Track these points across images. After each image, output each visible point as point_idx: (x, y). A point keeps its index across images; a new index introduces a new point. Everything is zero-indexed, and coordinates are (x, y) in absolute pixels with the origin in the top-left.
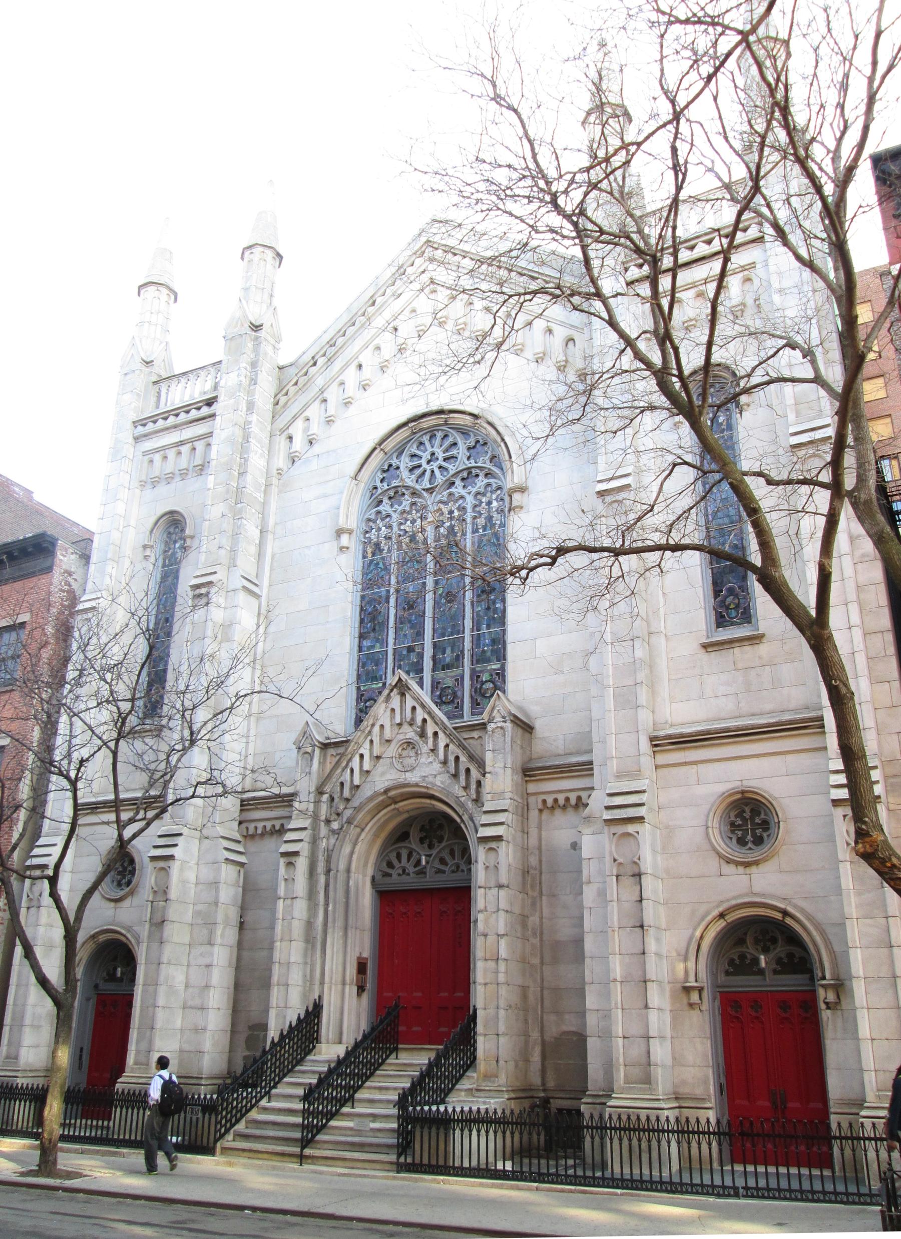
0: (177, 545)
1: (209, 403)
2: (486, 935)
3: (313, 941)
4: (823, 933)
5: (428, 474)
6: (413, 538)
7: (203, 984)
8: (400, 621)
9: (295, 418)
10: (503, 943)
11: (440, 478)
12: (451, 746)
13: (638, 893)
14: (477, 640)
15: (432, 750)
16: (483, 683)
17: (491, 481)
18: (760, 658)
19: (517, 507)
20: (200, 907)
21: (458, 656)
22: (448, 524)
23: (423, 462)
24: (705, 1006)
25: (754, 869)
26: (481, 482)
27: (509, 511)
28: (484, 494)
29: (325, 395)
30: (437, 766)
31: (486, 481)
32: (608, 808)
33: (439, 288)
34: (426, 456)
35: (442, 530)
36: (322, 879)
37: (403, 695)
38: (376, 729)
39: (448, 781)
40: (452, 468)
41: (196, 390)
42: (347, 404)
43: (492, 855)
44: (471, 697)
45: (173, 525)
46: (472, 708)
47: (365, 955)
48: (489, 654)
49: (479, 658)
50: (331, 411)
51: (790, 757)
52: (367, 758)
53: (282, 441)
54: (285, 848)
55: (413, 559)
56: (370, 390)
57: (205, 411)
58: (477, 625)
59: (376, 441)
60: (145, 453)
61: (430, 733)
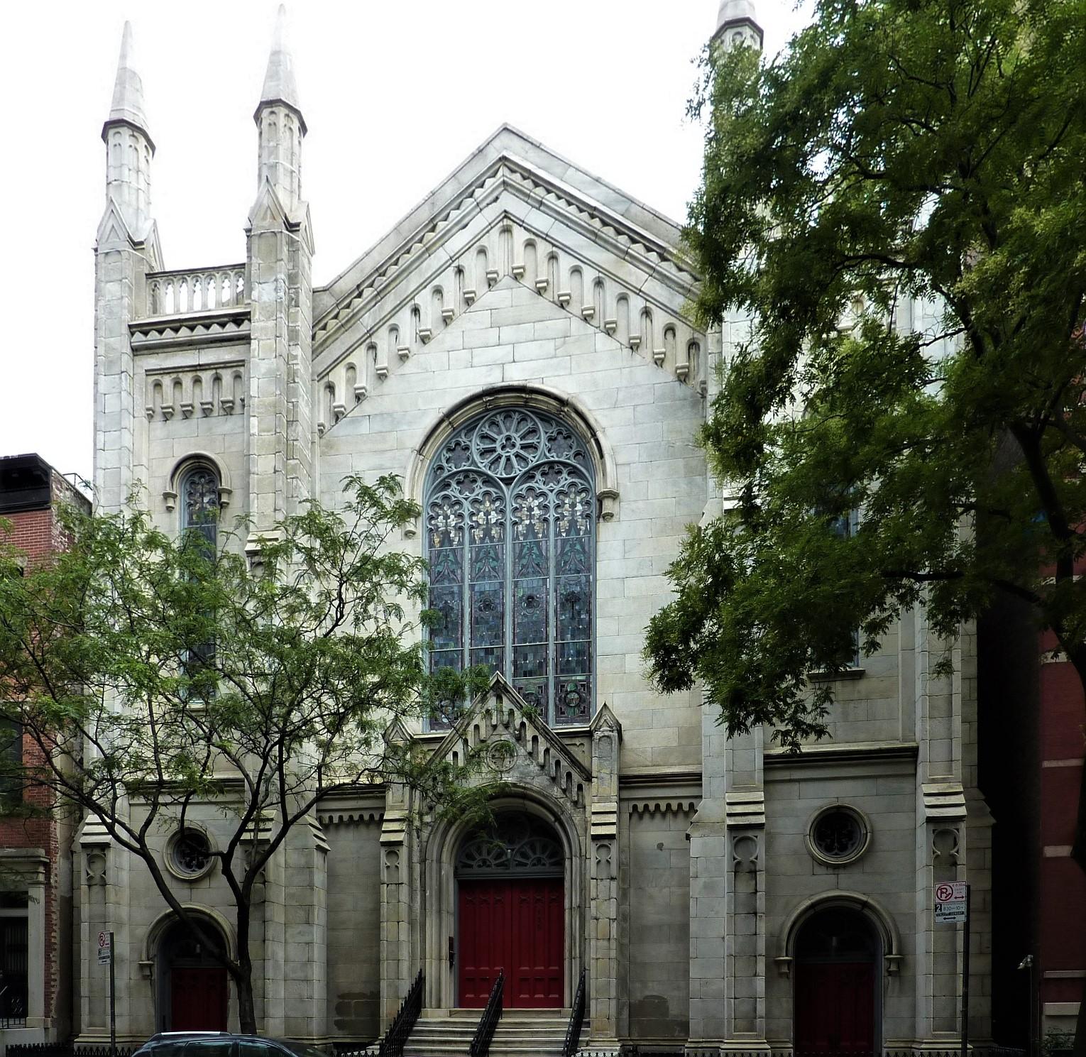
0: (206, 500)
1: (238, 319)
2: (597, 919)
3: (417, 926)
4: (894, 920)
5: (503, 460)
6: (487, 532)
7: (305, 959)
8: (476, 622)
9: (336, 362)
10: (614, 925)
11: (518, 469)
12: (552, 751)
13: (753, 887)
14: (561, 649)
15: (530, 754)
16: (567, 693)
17: (491, 490)
18: (859, 692)
19: (608, 514)
20: (292, 890)
21: (541, 663)
22: (527, 522)
23: (498, 445)
24: (791, 976)
25: (841, 871)
26: (565, 479)
27: (599, 517)
28: (566, 494)
29: (374, 339)
30: (534, 768)
31: (570, 480)
32: (730, 815)
33: (516, 229)
34: (500, 440)
35: (520, 528)
36: (417, 868)
37: (499, 698)
38: (471, 728)
39: (548, 783)
40: (533, 459)
41: (213, 298)
42: (403, 358)
43: (603, 851)
44: (556, 706)
45: (198, 473)
46: (557, 716)
47: (452, 935)
48: (574, 664)
49: (564, 668)
50: (383, 362)
51: (880, 781)
52: (461, 756)
53: (322, 394)
54: (384, 838)
55: (487, 556)
56: (432, 344)
57: (231, 329)
58: (561, 633)
59: (445, 410)
60: (149, 372)
61: (529, 737)
